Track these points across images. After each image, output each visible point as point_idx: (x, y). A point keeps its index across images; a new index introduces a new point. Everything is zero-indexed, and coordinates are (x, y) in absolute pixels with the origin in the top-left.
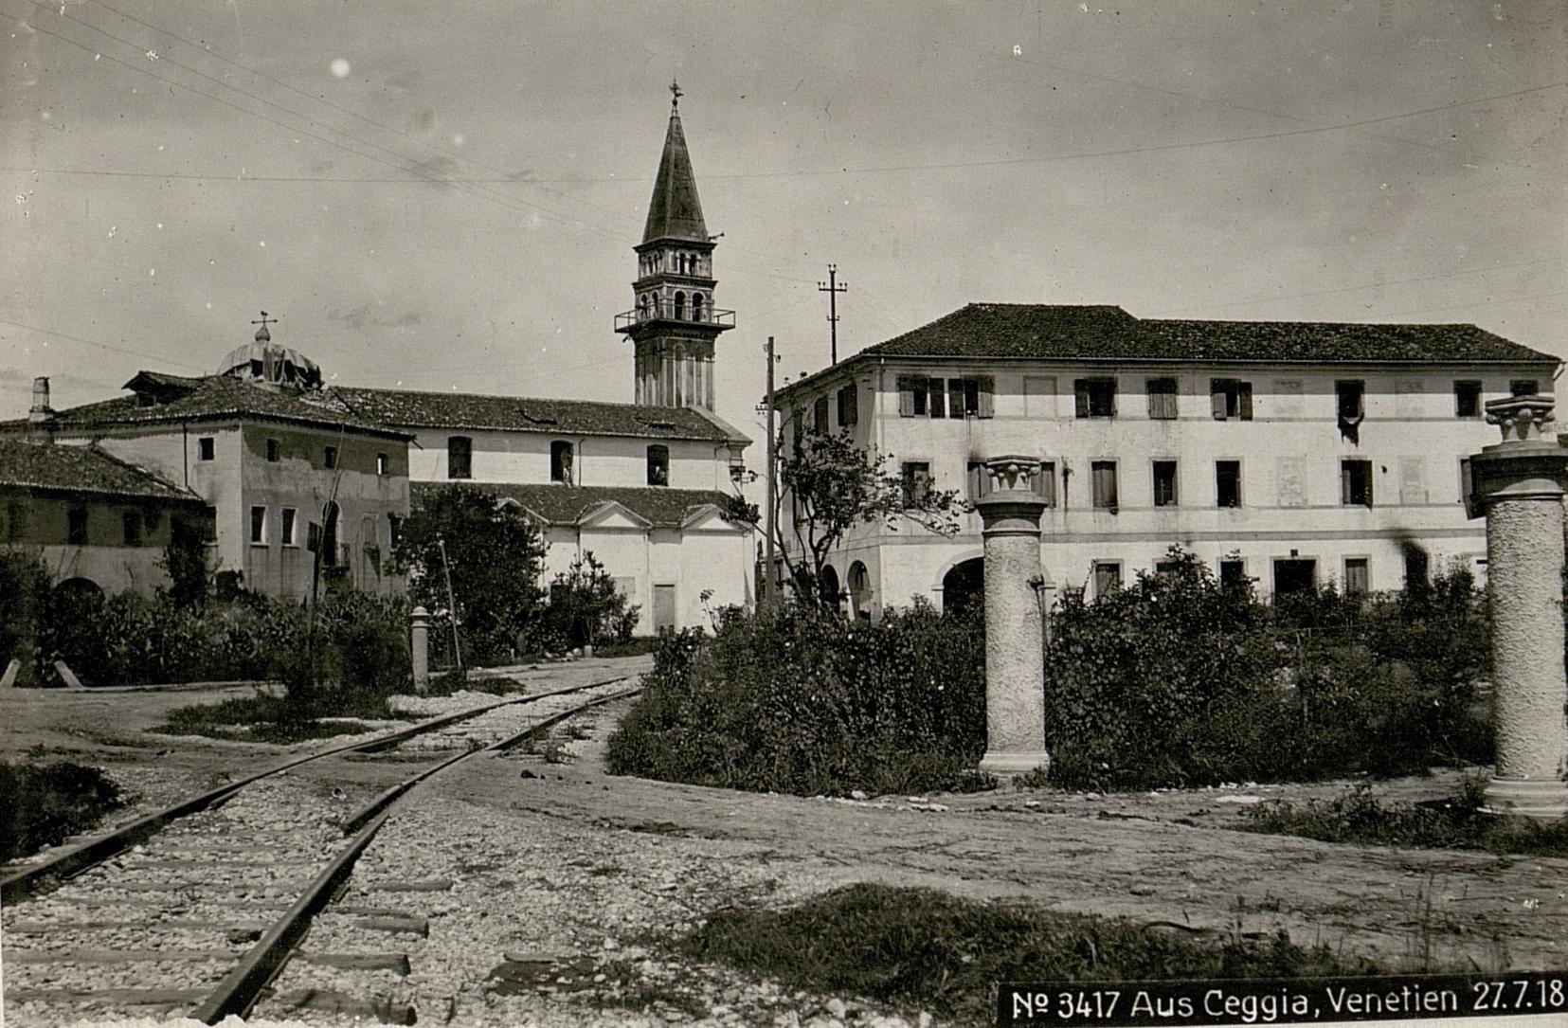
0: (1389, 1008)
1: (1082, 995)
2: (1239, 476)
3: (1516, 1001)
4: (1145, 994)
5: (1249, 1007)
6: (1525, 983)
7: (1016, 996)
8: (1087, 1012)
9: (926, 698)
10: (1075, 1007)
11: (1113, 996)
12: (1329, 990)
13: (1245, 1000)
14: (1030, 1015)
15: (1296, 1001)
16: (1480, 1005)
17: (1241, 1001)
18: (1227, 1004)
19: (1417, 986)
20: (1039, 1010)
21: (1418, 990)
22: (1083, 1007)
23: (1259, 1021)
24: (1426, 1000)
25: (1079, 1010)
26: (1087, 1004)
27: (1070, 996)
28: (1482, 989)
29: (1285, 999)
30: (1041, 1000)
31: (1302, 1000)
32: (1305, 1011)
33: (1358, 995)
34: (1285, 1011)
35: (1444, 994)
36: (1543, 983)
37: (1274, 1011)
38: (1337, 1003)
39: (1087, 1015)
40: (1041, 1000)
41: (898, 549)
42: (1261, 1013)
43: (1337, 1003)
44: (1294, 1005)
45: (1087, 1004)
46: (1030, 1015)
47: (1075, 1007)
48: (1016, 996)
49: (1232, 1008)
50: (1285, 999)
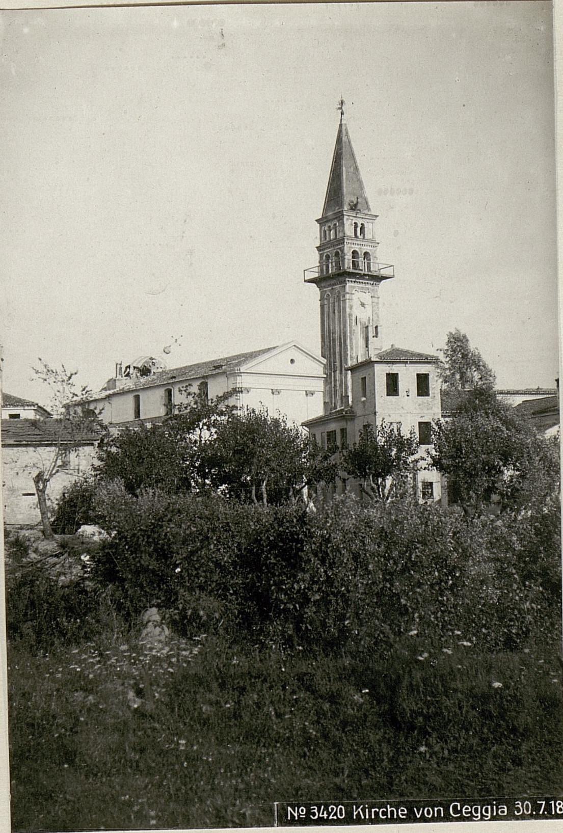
0: (401, 816)
1: (323, 807)
2: (10, 749)
3: (540, 810)
4: (343, 807)
5: (476, 812)
6: (544, 803)
7: (289, 809)
8: (325, 816)
9: (298, 535)
10: (319, 813)
11: (542, 804)
12: (415, 809)
13: (484, 808)
14: (296, 818)
15: (501, 808)
16: (418, 814)
17: (472, 809)
18: (464, 810)
19: (367, 806)
20: (301, 816)
21: (496, 805)
22: (323, 814)
23: (482, 819)
24: (400, 812)
25: (321, 816)
26: (325, 812)
27: (316, 808)
28: (333, 809)
29: (495, 807)
30: (302, 811)
31: (504, 808)
32: (506, 814)
33: (405, 810)
34: (495, 814)
35: (436, 809)
36: (553, 802)
37: (489, 815)
38: (295, 812)
39: (325, 818)
40: (302, 811)
41: (130, 420)
42: (482, 815)
43: (295, 812)
44: (500, 810)
45: (325, 812)
46: (296, 818)
47: (319, 813)
48: (289, 809)
49: (466, 813)
50: (495, 807)
